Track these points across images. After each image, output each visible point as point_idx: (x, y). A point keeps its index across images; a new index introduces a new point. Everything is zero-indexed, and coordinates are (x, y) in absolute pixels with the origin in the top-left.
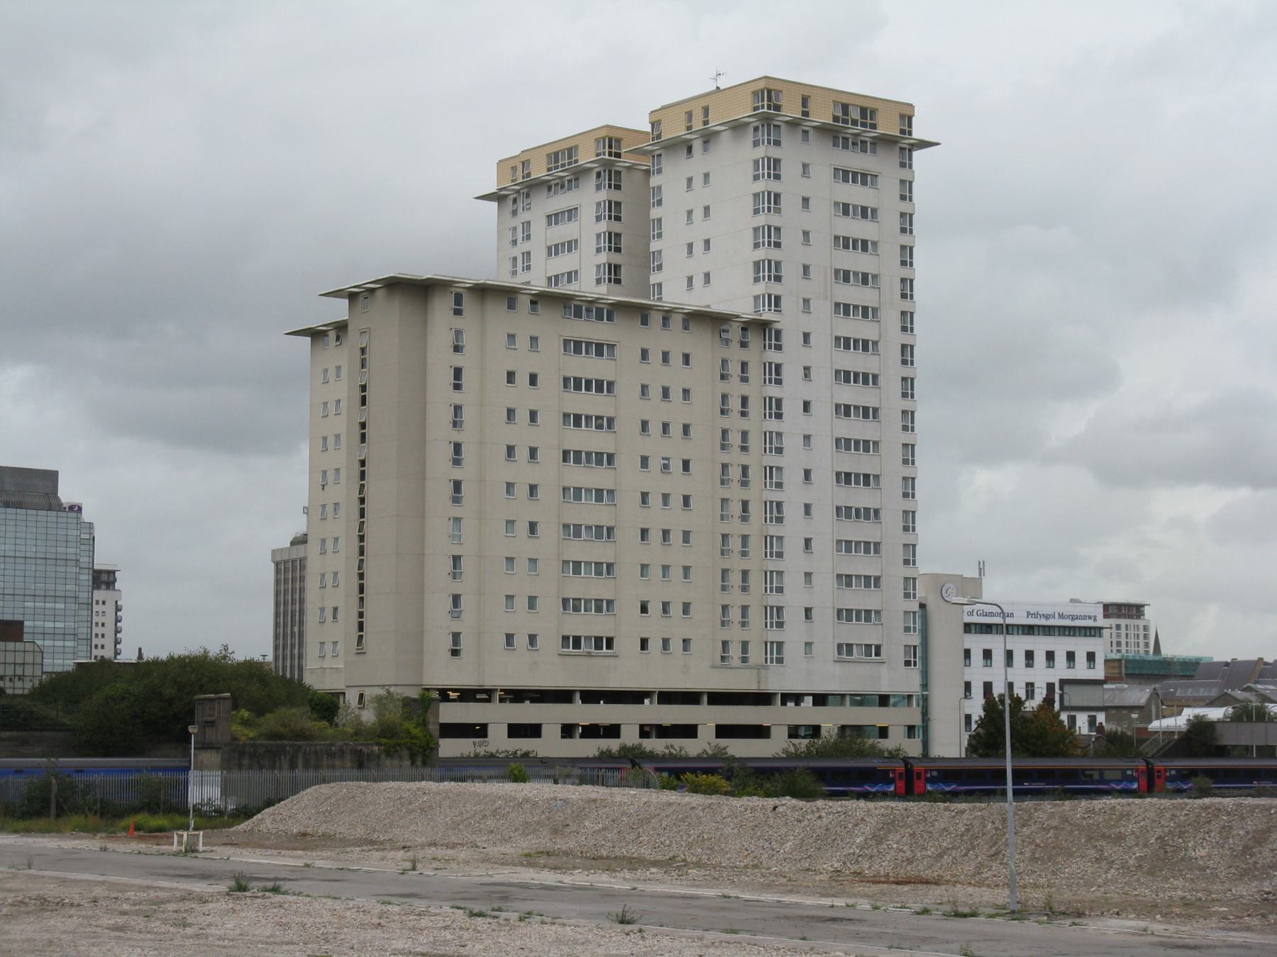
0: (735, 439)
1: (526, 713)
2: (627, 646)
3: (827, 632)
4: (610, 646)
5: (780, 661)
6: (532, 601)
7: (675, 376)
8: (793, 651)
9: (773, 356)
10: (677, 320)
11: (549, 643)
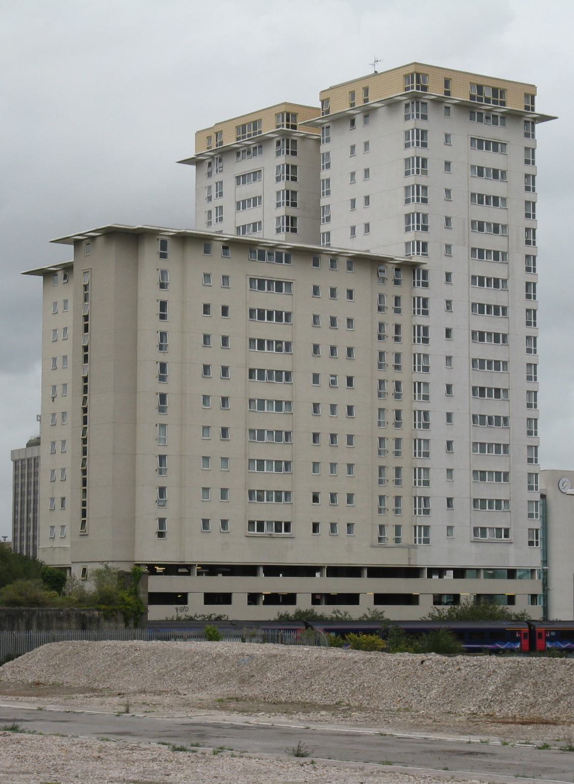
0: (390, 360)
1: (219, 584)
2: (301, 528)
3: (466, 518)
4: (506, 536)
5: (427, 541)
6: (224, 492)
7: (341, 308)
8: (437, 534)
9: (421, 292)
10: (342, 262)
11: (238, 527)
